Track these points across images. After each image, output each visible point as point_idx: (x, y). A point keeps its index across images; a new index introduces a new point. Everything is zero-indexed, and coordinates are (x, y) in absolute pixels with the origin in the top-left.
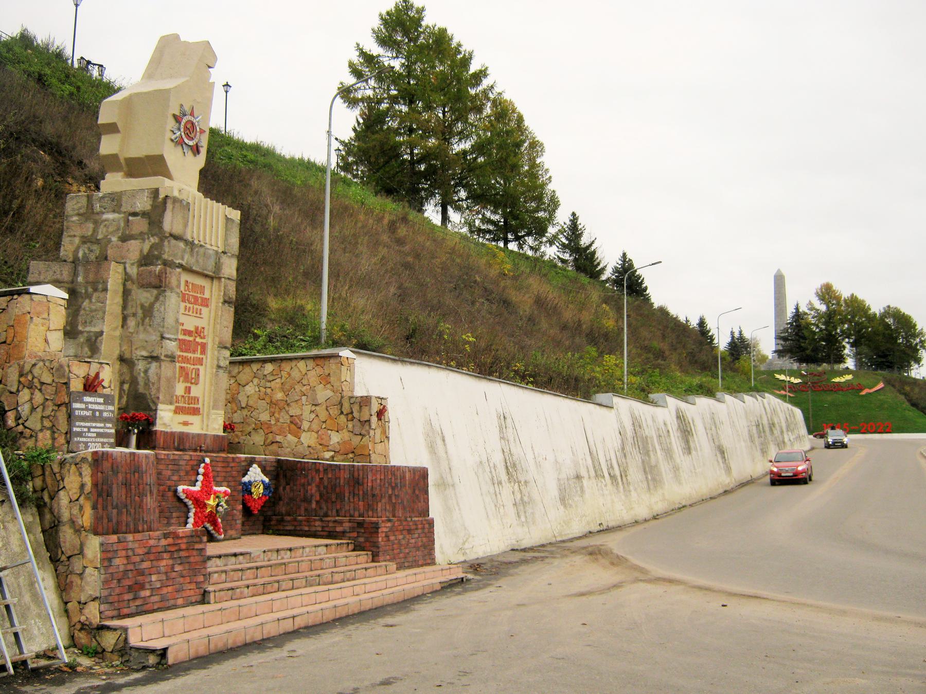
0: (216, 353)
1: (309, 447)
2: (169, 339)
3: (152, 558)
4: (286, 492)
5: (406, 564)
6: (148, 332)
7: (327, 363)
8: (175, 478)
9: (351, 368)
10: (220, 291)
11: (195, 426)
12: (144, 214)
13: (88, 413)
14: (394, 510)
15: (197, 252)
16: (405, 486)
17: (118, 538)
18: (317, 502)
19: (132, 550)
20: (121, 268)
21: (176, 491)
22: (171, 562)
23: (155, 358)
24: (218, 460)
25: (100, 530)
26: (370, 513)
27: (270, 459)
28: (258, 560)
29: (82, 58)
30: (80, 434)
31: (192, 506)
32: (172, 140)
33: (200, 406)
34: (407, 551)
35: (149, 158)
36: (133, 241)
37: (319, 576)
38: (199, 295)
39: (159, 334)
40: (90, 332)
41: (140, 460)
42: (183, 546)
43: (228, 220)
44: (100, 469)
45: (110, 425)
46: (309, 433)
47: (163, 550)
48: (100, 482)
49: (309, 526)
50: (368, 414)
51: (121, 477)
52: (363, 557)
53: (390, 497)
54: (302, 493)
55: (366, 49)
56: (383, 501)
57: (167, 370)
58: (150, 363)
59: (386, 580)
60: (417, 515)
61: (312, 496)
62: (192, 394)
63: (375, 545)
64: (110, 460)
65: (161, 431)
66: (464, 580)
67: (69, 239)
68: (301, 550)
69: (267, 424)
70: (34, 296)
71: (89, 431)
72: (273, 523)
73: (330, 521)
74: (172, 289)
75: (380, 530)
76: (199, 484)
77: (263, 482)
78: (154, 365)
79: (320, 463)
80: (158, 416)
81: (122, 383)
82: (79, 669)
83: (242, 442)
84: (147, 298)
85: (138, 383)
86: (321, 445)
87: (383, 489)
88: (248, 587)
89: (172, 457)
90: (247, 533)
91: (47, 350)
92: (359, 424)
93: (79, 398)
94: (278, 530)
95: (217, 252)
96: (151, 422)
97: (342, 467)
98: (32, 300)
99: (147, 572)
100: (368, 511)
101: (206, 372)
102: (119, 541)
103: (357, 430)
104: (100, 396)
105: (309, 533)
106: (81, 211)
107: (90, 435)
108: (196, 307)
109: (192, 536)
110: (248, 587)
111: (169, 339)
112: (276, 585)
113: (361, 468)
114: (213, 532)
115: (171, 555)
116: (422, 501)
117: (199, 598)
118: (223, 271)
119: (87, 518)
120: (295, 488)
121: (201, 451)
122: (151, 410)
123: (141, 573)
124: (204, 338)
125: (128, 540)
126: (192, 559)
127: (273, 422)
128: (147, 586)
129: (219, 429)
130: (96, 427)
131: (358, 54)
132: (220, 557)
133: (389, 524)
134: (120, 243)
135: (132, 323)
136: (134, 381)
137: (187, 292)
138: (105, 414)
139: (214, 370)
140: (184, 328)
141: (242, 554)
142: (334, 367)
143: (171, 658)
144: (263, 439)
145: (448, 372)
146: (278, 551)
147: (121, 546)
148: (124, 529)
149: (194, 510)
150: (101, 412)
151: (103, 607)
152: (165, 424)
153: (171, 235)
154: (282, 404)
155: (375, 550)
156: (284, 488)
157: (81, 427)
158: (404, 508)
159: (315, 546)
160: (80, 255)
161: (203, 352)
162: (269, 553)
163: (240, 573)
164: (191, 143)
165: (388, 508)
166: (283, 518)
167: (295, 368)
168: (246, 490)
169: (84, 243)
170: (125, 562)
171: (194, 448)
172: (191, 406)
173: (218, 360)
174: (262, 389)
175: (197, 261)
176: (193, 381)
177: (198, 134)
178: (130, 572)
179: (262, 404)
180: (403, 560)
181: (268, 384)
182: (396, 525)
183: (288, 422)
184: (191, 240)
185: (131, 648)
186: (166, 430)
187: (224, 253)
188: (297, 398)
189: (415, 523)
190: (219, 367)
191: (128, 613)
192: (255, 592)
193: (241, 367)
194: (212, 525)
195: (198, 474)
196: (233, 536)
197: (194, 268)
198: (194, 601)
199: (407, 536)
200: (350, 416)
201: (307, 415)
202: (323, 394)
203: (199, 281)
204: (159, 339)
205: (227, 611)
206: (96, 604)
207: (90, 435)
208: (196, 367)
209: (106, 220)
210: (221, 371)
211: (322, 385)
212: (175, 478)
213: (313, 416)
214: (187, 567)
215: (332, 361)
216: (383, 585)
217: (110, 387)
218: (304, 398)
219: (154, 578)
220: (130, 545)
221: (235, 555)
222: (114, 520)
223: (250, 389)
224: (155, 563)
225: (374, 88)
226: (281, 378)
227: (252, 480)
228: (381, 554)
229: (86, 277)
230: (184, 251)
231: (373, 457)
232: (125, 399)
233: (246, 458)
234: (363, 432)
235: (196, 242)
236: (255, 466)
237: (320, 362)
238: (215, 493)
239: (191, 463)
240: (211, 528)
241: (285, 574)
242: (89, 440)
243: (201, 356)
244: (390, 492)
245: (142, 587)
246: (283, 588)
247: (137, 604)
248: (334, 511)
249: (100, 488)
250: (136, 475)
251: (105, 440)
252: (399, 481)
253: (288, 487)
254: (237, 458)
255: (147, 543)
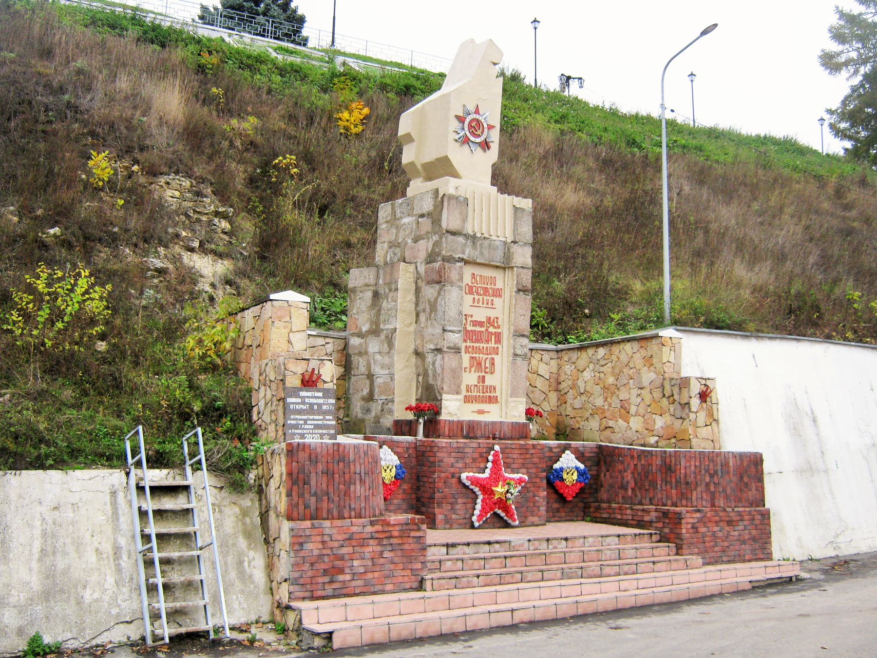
0: (512, 341)
1: (637, 432)
2: (451, 331)
3: (355, 544)
4: (606, 479)
5: (725, 559)
6: (434, 326)
7: (649, 344)
8: (460, 465)
9: (675, 347)
10: (512, 278)
11: (493, 414)
12: (429, 214)
13: (304, 407)
14: (713, 499)
15: (481, 245)
16: (728, 473)
17: (313, 524)
18: (633, 489)
19: (330, 536)
20: (412, 268)
21: (459, 478)
22: (379, 548)
23: (439, 350)
24: (513, 447)
25: (295, 515)
26: (684, 502)
27: (590, 445)
28: (521, 548)
29: (562, 75)
30: (296, 427)
31: (479, 493)
32: (456, 141)
33: (498, 394)
34: (726, 544)
35: (438, 160)
36: (421, 241)
37: (582, 568)
38: (489, 286)
39: (441, 328)
40: (388, 329)
41: (346, 450)
42: (396, 534)
43: (516, 209)
44: (295, 458)
45: (331, 418)
46: (637, 417)
47: (369, 536)
48: (295, 471)
49: (621, 514)
50: (687, 395)
51: (320, 467)
52: (663, 550)
53: (707, 485)
54: (619, 480)
55: (846, 10)
56: (699, 489)
57: (450, 360)
58: (436, 355)
59: (672, 576)
60: (747, 505)
61: (628, 483)
62: (487, 383)
63: (679, 536)
64: (307, 450)
65: (445, 420)
66: (794, 579)
67: (381, 245)
68: (582, 540)
69: (601, 409)
70: (274, 302)
71: (306, 423)
72: (592, 510)
73: (638, 510)
74: (452, 284)
75: (683, 521)
76: (488, 471)
77: (577, 469)
78: (439, 356)
79: (634, 449)
80: (443, 405)
81: (418, 375)
82: (167, 647)
83: (581, 427)
84: (432, 294)
85: (428, 376)
86: (647, 429)
87: (699, 477)
88: (478, 576)
89: (455, 445)
90: (563, 519)
91: (291, 349)
92: (679, 407)
93: (294, 392)
94: (595, 517)
95: (505, 243)
96: (438, 413)
97: (654, 453)
98: (273, 305)
99: (347, 557)
100: (681, 500)
101: (502, 361)
102: (313, 527)
103: (678, 414)
104: (319, 391)
105: (621, 521)
106: (388, 219)
107: (306, 427)
108: (485, 298)
109: (407, 524)
110: (478, 576)
111: (451, 331)
112: (519, 576)
113: (673, 454)
114: (505, 518)
115: (379, 542)
116: (754, 489)
117: (415, 585)
118: (514, 260)
119: (283, 506)
120: (614, 474)
121: (494, 438)
122: (437, 400)
123: (341, 558)
124: (499, 327)
125: (324, 526)
126: (406, 547)
127: (606, 407)
128: (347, 570)
129: (520, 416)
130: (313, 420)
131: (837, 16)
132: (435, 545)
133: (698, 515)
134: (413, 244)
135: (423, 318)
136: (426, 374)
137: (475, 285)
138: (324, 407)
139: (511, 358)
140: (473, 319)
141: (497, 542)
142: (655, 348)
143: (337, 643)
144: (598, 424)
145: (828, 345)
146: (548, 540)
147: (315, 532)
148: (325, 515)
149: (481, 497)
150: (320, 405)
151: (292, 588)
152: (450, 413)
153: (448, 232)
154: (613, 388)
155: (678, 542)
156: (605, 475)
157: (297, 419)
158: (727, 497)
159: (602, 537)
160: (388, 259)
161: (498, 340)
162: (537, 542)
163: (482, 562)
164: (478, 140)
165: (705, 497)
166: (599, 505)
167: (623, 352)
168: (557, 476)
169: (390, 247)
170: (320, 546)
171: (487, 435)
172: (486, 394)
173: (514, 348)
174: (597, 375)
175: (482, 254)
176: (488, 370)
177: (486, 130)
178: (326, 557)
179: (598, 389)
180: (719, 554)
181: (602, 369)
182: (709, 515)
183: (619, 407)
184: (472, 234)
185: (304, 629)
186: (451, 419)
187: (514, 242)
188: (626, 381)
189: (740, 514)
190: (516, 355)
191: (323, 595)
192: (488, 582)
193: (579, 353)
194: (504, 511)
195: (488, 461)
196: (535, 523)
197: (478, 261)
198: (408, 587)
199: (727, 528)
200: (671, 399)
201: (635, 400)
202: (648, 377)
203: (488, 273)
204: (442, 331)
205: (432, 600)
206: (285, 586)
207: (306, 427)
208: (490, 356)
209: (404, 224)
210: (519, 360)
211: (646, 368)
212: (460, 465)
213: (639, 399)
214: (399, 553)
215: (654, 341)
216: (702, 577)
217: (332, 381)
218: (631, 381)
219: (356, 563)
220: (327, 531)
221: (489, 543)
222: (313, 507)
223: (587, 375)
224: (358, 549)
225: (858, 50)
226: (612, 362)
227: (565, 466)
228: (685, 546)
229: (384, 280)
230: (465, 245)
231: (694, 442)
232: (420, 391)
233: (559, 444)
234: (684, 416)
235: (478, 235)
236: (567, 452)
237: (644, 343)
238: (505, 480)
239: (481, 450)
240: (503, 514)
241: (546, 564)
242: (305, 431)
243: (496, 346)
244: (708, 479)
245: (341, 571)
246: (529, 579)
247: (334, 587)
248: (648, 500)
249: (294, 476)
250: (341, 465)
251: (324, 431)
252: (719, 467)
253: (607, 473)
254: (539, 444)
255: (348, 529)
